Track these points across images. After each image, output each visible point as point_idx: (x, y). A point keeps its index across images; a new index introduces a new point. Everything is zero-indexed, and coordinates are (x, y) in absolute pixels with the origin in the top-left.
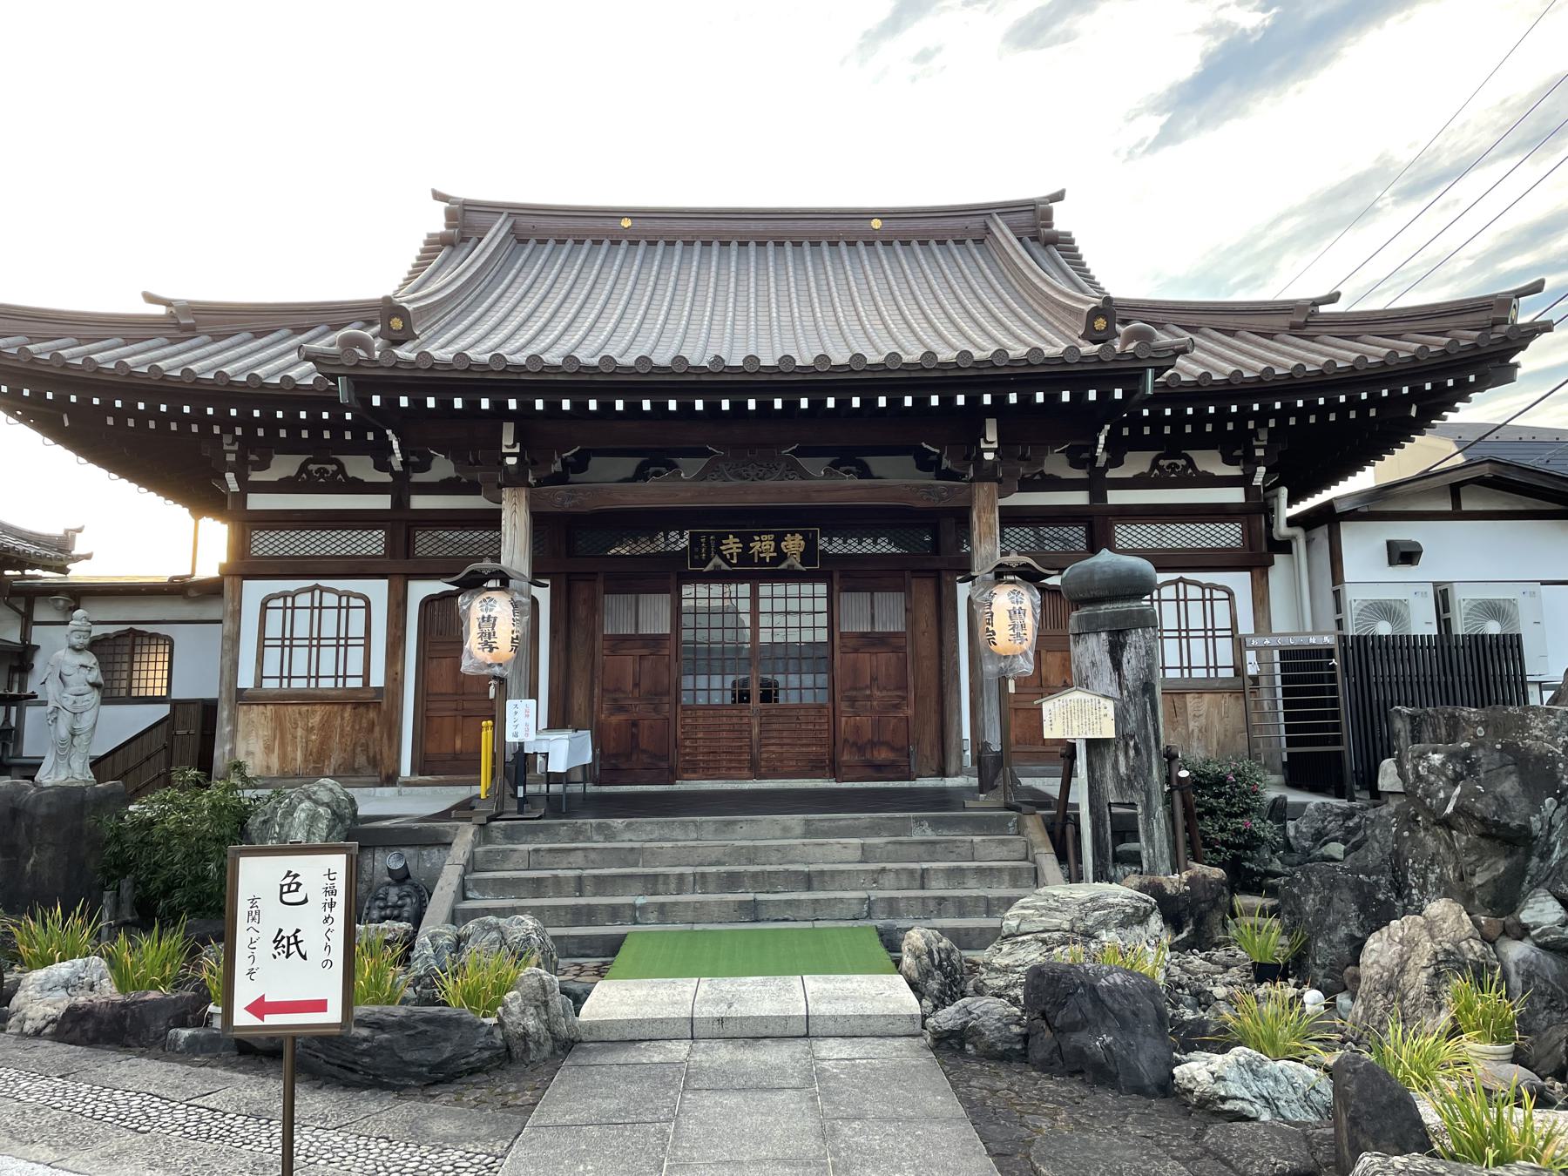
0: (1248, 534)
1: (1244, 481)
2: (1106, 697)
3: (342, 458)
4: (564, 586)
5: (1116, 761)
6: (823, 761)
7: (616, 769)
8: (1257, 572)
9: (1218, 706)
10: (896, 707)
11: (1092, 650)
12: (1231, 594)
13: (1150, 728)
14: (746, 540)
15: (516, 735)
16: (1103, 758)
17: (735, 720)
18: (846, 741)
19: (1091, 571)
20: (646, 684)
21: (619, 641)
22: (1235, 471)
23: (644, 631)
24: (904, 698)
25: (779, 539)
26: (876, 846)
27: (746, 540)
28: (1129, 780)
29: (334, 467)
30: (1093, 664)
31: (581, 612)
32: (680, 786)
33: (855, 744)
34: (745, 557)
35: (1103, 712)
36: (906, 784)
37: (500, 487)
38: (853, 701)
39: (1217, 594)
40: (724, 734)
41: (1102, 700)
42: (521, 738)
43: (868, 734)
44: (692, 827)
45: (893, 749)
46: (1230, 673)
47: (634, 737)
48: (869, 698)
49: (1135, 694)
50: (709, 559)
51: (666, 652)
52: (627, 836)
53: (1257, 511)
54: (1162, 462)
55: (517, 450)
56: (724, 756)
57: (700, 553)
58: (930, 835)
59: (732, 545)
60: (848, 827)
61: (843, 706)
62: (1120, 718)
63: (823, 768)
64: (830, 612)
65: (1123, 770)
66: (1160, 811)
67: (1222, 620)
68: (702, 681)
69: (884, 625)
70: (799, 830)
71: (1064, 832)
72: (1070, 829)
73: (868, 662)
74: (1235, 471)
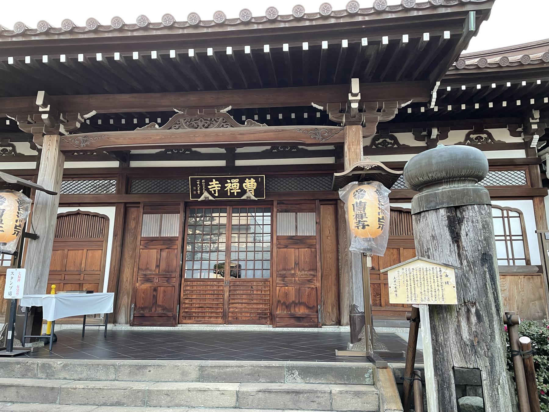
0: (530, 177)
1: (525, 146)
2: (446, 265)
3: (15, 143)
4: (122, 210)
5: (459, 326)
6: (266, 314)
7: (143, 317)
8: (537, 200)
9: (517, 285)
10: (310, 281)
11: (434, 224)
12: (520, 214)
13: (491, 296)
14: (223, 182)
15: (10, 294)
16: (445, 322)
17: (215, 288)
18: (279, 301)
19: (430, 158)
20: (163, 266)
21: (150, 242)
22: (519, 140)
23: (163, 235)
24: (314, 276)
25: (242, 182)
26: (248, 394)
27: (223, 182)
28: (473, 346)
29: (11, 148)
30: (433, 237)
31: (132, 224)
32: (180, 328)
33: (284, 303)
34: (223, 192)
35: (445, 279)
36: (315, 330)
37: (44, 135)
38: (283, 277)
39: (511, 214)
40: (208, 297)
41: (444, 269)
42: (14, 296)
43: (292, 298)
44: (112, 370)
45: (308, 307)
46: (523, 263)
47: (155, 297)
48: (293, 275)
49: (474, 263)
50: (202, 193)
51: (175, 247)
52: (63, 375)
53: (535, 162)
54: (472, 136)
55: (48, 109)
56: (207, 310)
57: (197, 190)
58: (300, 384)
59: (215, 185)
60: (234, 373)
61: (278, 280)
62: (462, 285)
63: (266, 318)
64: (272, 225)
65: (465, 335)
66: (504, 376)
67: (516, 229)
68: (258, 275)
69: (303, 232)
70: (194, 374)
71: (411, 385)
72: (417, 385)
73: (293, 253)
74: (519, 140)
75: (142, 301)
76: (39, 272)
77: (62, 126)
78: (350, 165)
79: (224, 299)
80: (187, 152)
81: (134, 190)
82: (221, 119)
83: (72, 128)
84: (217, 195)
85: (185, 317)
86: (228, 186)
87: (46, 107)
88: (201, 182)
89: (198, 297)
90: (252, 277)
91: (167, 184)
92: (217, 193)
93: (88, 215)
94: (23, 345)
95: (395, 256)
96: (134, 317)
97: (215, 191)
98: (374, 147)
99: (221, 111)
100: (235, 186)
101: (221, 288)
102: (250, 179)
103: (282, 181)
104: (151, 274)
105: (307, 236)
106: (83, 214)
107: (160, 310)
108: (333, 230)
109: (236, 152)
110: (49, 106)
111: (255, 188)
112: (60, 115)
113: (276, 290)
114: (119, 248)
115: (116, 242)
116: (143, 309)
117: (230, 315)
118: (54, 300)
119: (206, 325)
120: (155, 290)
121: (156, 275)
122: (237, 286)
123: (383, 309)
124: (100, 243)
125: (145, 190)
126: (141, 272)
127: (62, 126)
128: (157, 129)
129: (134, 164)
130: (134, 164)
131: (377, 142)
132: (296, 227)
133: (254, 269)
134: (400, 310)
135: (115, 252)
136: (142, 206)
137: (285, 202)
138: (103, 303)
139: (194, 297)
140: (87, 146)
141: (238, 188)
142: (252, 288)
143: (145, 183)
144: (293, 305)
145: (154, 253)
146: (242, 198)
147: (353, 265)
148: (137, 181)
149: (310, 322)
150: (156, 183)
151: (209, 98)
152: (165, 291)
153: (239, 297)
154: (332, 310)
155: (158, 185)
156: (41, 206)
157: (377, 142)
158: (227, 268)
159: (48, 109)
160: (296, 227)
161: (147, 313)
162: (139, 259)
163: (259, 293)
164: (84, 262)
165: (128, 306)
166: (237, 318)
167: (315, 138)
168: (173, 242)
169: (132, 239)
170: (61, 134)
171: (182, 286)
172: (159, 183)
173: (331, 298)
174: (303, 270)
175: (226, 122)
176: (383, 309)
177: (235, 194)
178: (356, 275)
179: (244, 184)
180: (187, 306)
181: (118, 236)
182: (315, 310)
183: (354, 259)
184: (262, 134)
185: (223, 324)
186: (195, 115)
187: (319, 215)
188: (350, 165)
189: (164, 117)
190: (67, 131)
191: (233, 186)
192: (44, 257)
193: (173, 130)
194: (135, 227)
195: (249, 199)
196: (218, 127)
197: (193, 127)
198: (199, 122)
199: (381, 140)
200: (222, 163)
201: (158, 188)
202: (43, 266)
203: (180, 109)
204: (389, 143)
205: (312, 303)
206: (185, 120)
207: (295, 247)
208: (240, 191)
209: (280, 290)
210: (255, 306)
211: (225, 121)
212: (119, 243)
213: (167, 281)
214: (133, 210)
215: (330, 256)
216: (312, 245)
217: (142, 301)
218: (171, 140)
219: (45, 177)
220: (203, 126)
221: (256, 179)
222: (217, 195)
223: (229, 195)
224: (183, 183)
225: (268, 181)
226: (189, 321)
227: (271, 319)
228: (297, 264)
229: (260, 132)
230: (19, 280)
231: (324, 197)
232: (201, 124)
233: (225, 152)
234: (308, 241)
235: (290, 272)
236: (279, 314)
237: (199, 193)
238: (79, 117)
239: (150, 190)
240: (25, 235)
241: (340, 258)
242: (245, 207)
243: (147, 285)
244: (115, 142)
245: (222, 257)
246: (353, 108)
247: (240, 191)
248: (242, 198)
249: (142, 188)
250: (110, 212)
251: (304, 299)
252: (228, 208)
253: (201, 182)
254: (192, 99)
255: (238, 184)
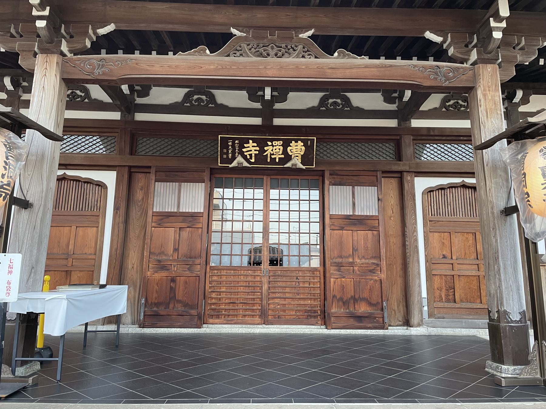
4: (126, 176)
6: (315, 312)
7: (156, 315)
14: (262, 144)
17: (249, 279)
18: (334, 296)
20: (183, 249)
21: (165, 218)
27: (262, 144)
31: (139, 195)
32: (207, 329)
33: (341, 299)
34: (261, 157)
36: (381, 332)
40: (241, 289)
43: (350, 292)
45: (370, 304)
48: (352, 264)
50: (234, 158)
55: (46, 13)
57: (227, 153)
59: (251, 148)
63: (315, 317)
69: (362, 209)
75: (155, 295)
76: (34, 258)
77: (64, 42)
78: (487, 117)
79: (262, 293)
80: (210, 105)
81: (140, 150)
82: (300, 47)
83: (78, 46)
84: (253, 160)
85: (212, 316)
86: (269, 150)
87: (44, 9)
88: (233, 143)
89: (228, 290)
90: (297, 266)
91: (185, 145)
92: (253, 158)
93: (77, 181)
94: (13, 372)
95: (471, 242)
96: (145, 315)
97: (251, 155)
98: (444, 110)
99: (301, 36)
100: (278, 150)
101: (258, 279)
102: (296, 142)
103: (332, 147)
104: (166, 260)
105: (367, 216)
106: (71, 180)
107: (180, 308)
108: (397, 209)
109: (274, 108)
110: (48, 8)
111: (302, 153)
112: (61, 26)
113: (330, 282)
114: (122, 226)
115: (117, 217)
116: (157, 305)
117: (270, 312)
118: (65, 303)
119: (240, 326)
120: (173, 280)
121: (174, 260)
122: (279, 276)
123: (457, 306)
124: (94, 218)
125: (155, 151)
126: (154, 257)
127: (64, 42)
128: (208, 55)
129: (140, 117)
130: (140, 117)
131: (447, 104)
132: (354, 204)
133: (299, 256)
134: (478, 307)
135: (116, 231)
136: (154, 172)
137: (340, 173)
138: (118, 300)
139: (224, 290)
140: (104, 74)
141: (281, 153)
142: (297, 278)
143: (155, 142)
144: (352, 301)
145: (171, 233)
146: (285, 166)
147: (500, 255)
148: (145, 140)
149: (374, 322)
150: (170, 143)
151: (283, 16)
152: (186, 282)
153: (281, 290)
154: (398, 307)
155: (173, 145)
156: (34, 158)
157: (447, 104)
158: (266, 254)
159: (46, 13)
160: (354, 204)
161: (162, 311)
162: (151, 240)
163: (307, 285)
164: (72, 242)
165: (134, 301)
166: (279, 317)
167: (435, 79)
168: (195, 219)
169: (139, 213)
170: (63, 54)
171: (208, 275)
172: (174, 143)
173: (396, 294)
174: (363, 257)
175: (308, 51)
176: (457, 306)
177: (277, 160)
178: (504, 269)
179: (289, 148)
180: (213, 301)
181: (121, 210)
182: (380, 307)
183: (501, 247)
184: (361, 70)
185: (262, 324)
186: (264, 38)
187: (380, 190)
188: (487, 117)
189: (217, 41)
190: (71, 51)
191: (274, 150)
192: (40, 236)
193: (232, 58)
194: (143, 199)
195: (294, 167)
196: (297, 56)
197: (261, 55)
198: (269, 48)
199: (452, 102)
200: (257, 121)
201: (173, 149)
202: (39, 249)
203: (241, 29)
204: (461, 106)
205: (375, 298)
206: (248, 45)
207: (352, 229)
208: (283, 156)
209: (335, 283)
210: (302, 302)
211: (306, 49)
212: (122, 219)
213: (189, 269)
214: (140, 175)
215: (395, 241)
216: (374, 227)
217: (155, 295)
218: (231, 72)
219: (40, 116)
220: (276, 55)
221: (305, 142)
222: (253, 160)
223: (269, 161)
224: (206, 144)
225: (318, 144)
226: (217, 321)
227: (325, 319)
228: (355, 250)
229: (358, 67)
230: (10, 272)
231: (387, 168)
232: (272, 53)
233: (261, 107)
234: (369, 222)
235: (347, 260)
236: (336, 313)
237: (230, 157)
238: (90, 31)
239: (162, 151)
240: (14, 201)
241: (407, 243)
242: (286, 177)
243: (164, 274)
244: (147, 70)
245: (258, 239)
246: (495, 39)
247: (283, 156)
248: (285, 166)
249: (152, 148)
250: (109, 178)
251: (366, 295)
252: (265, 177)
253: (233, 143)
254: (259, 16)
255: (281, 148)
